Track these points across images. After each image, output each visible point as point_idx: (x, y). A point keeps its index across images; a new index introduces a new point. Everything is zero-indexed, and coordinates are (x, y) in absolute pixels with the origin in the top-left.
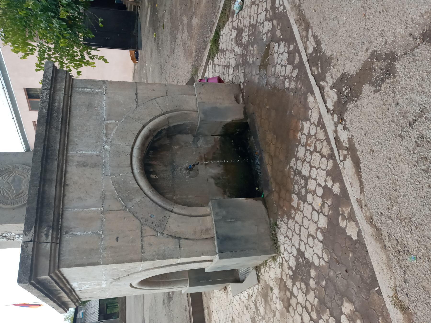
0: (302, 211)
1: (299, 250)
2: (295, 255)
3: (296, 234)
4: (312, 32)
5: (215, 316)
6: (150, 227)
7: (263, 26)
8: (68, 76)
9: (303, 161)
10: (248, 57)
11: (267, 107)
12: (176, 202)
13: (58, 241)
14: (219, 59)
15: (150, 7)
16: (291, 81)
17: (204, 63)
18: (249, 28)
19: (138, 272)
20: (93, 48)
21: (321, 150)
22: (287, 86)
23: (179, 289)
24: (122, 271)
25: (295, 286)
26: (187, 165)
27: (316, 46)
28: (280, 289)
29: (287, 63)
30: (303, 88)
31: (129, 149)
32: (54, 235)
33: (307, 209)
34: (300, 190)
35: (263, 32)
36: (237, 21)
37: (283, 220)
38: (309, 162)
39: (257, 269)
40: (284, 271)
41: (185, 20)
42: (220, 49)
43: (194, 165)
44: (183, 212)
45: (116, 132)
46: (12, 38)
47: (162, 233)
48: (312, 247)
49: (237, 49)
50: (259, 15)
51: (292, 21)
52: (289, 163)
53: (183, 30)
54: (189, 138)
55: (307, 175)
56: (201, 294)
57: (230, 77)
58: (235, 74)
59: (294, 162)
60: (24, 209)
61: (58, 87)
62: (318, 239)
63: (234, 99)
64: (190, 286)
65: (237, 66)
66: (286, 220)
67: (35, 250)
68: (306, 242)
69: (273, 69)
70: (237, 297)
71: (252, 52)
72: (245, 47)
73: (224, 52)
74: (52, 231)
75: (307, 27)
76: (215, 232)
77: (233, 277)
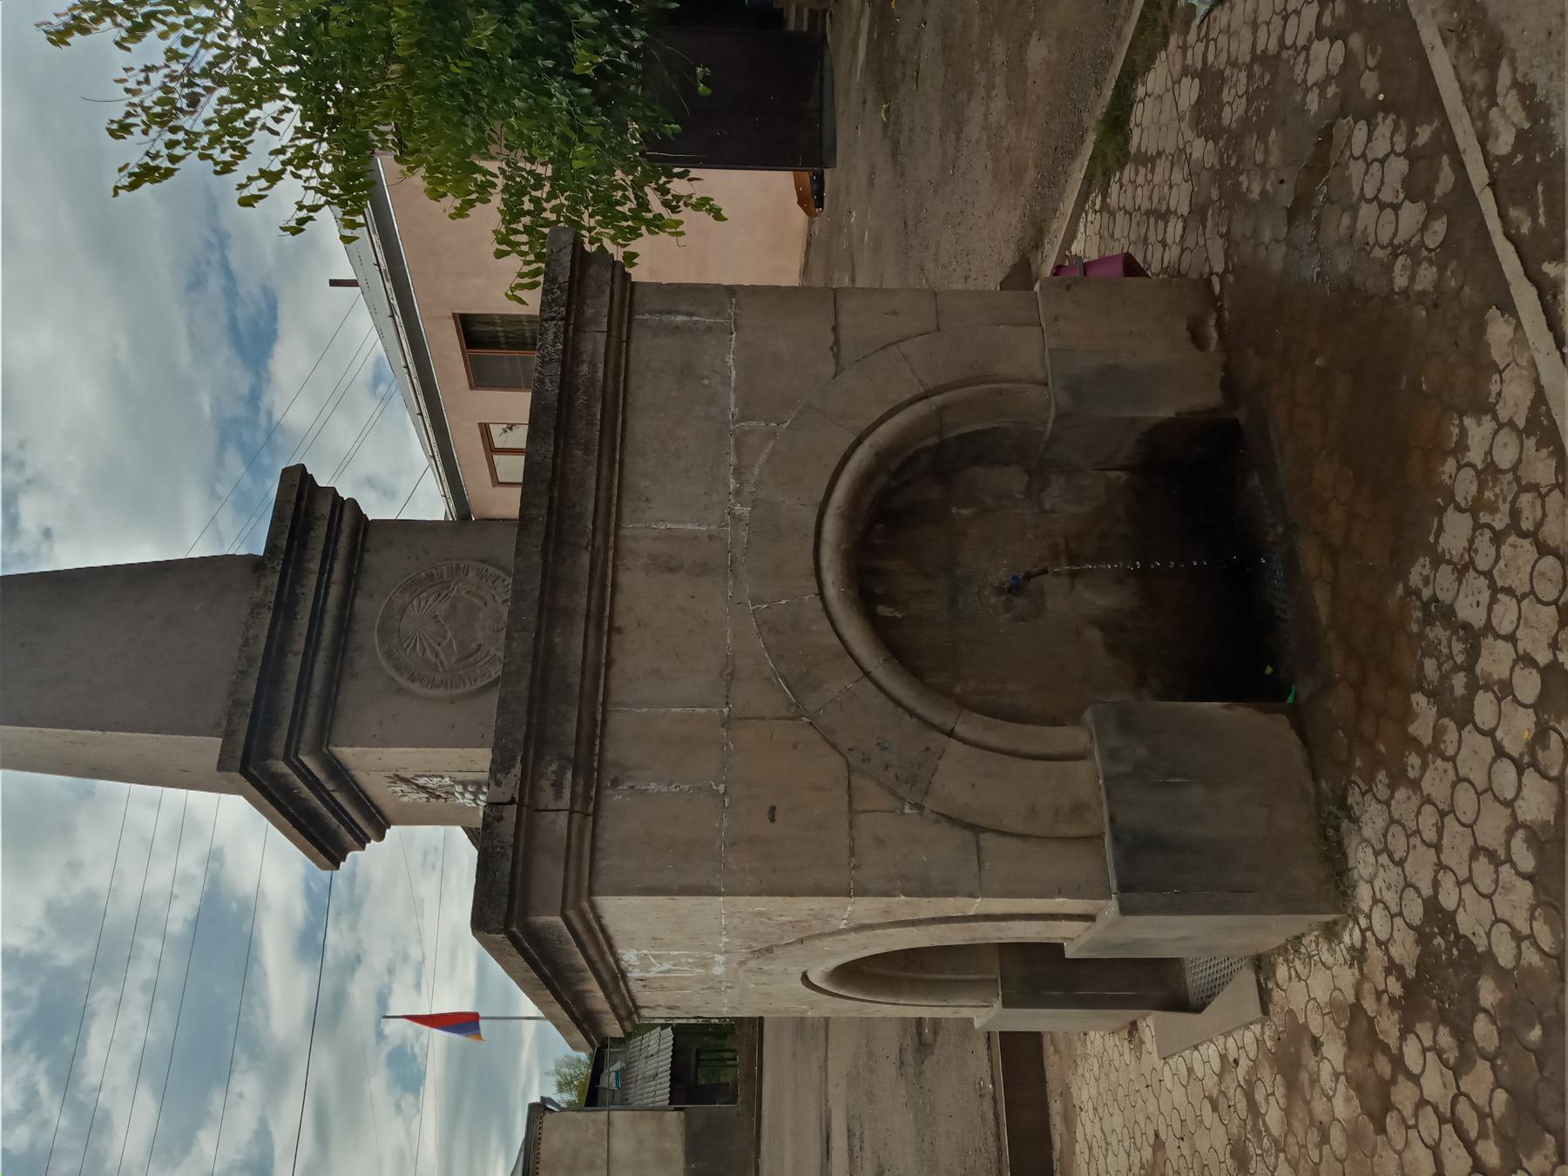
0: (1453, 759)
1: (1432, 906)
2: (1417, 921)
3: (1423, 841)
4: (1515, 70)
5: (1088, 1125)
6: (880, 784)
7: (1307, 61)
8: (618, 273)
9: (1463, 569)
10: (1243, 178)
11: (1318, 362)
12: (963, 704)
13: (589, 807)
14: (1129, 188)
15: (868, 10)
16: (1416, 264)
17: (1068, 206)
18: (1249, 68)
19: (832, 934)
20: (676, 170)
21: (1539, 525)
22: (1400, 281)
23: (966, 1013)
24: (782, 924)
25: (1411, 1039)
26: (1002, 575)
27: (1527, 126)
28: (1350, 1043)
29: (1402, 196)
30: (1467, 290)
31: (810, 515)
32: (580, 789)
33: (1473, 752)
34: (1445, 677)
35: (1305, 81)
36: (1201, 46)
37: (1370, 790)
38: (1488, 574)
39: (1261, 964)
40: (1368, 979)
41: (999, 53)
42: (1133, 151)
43: (1028, 576)
44: (992, 739)
45: (768, 461)
46: (429, 151)
47: (919, 807)
48: (1489, 897)
49: (1200, 149)
50: (1293, 20)
51: (1429, 34)
52: (1401, 574)
53: (991, 86)
54: (1014, 479)
55: (1477, 619)
56: (1037, 1037)
57: (1172, 255)
58: (1190, 243)
59: (1426, 572)
60: (494, 698)
61: (589, 312)
62: (1514, 865)
63: (1185, 334)
64: (1006, 1004)
65: (1198, 212)
66: (1382, 791)
67: (523, 831)
68: (1463, 873)
69: (1346, 220)
70: (1177, 1063)
71: (1259, 158)
72: (1231, 139)
73: (1147, 160)
74: (574, 777)
75: (1495, 52)
76: (1106, 819)
77: (1157, 987)
